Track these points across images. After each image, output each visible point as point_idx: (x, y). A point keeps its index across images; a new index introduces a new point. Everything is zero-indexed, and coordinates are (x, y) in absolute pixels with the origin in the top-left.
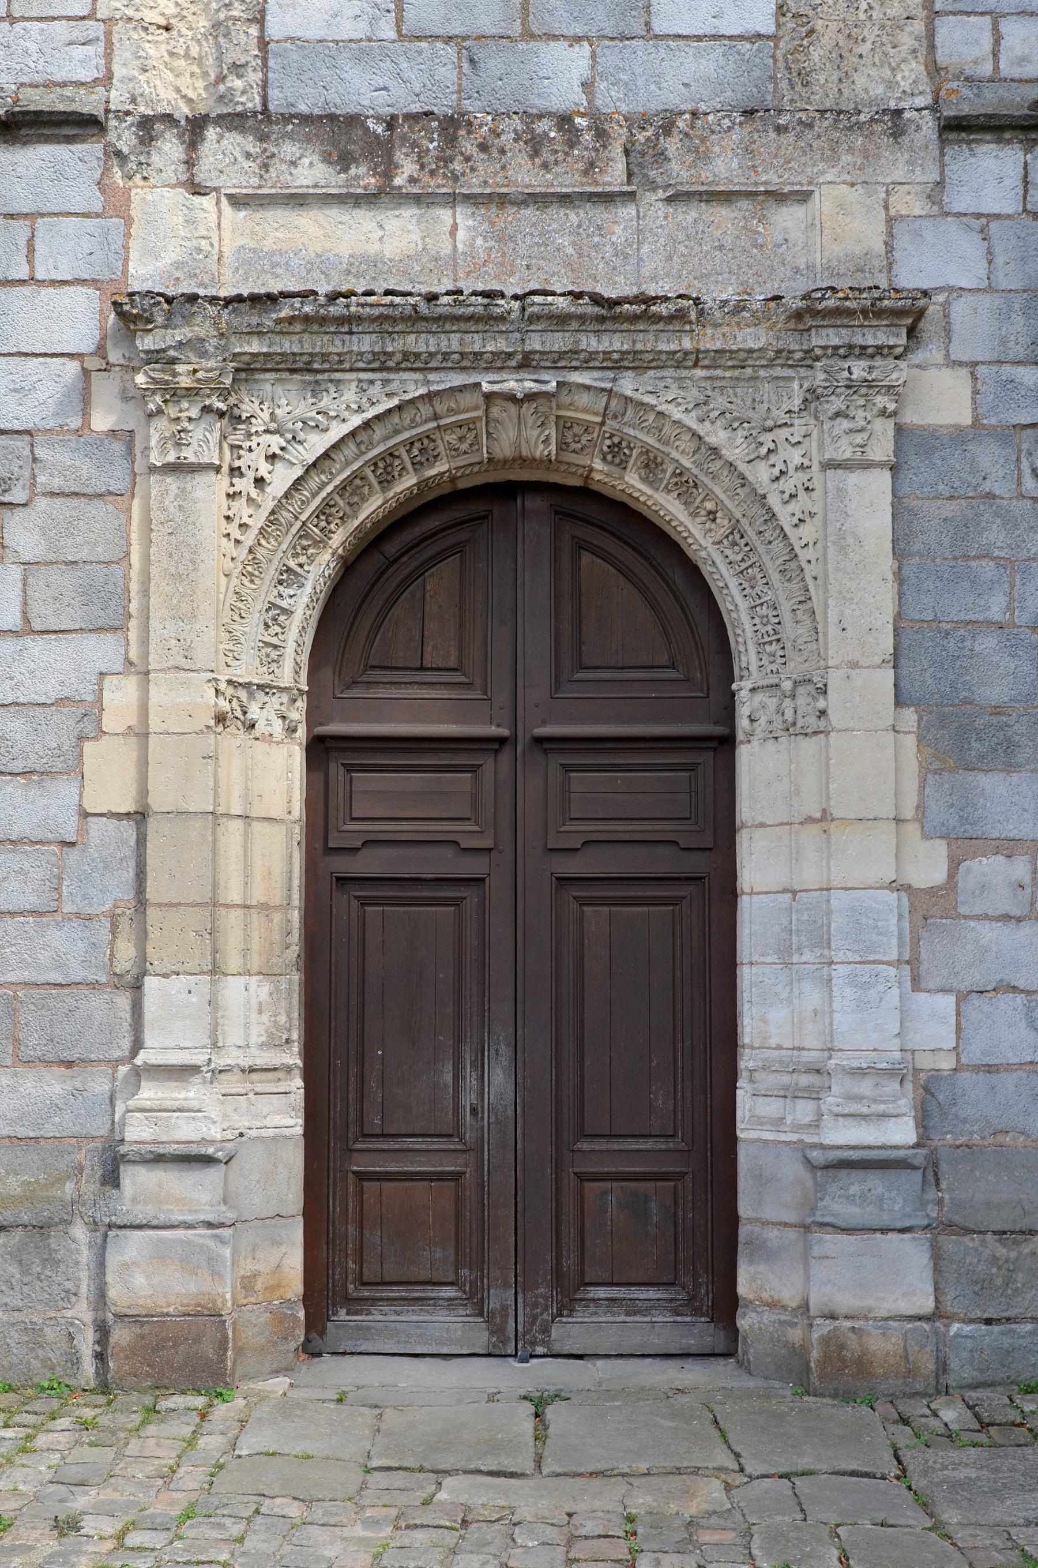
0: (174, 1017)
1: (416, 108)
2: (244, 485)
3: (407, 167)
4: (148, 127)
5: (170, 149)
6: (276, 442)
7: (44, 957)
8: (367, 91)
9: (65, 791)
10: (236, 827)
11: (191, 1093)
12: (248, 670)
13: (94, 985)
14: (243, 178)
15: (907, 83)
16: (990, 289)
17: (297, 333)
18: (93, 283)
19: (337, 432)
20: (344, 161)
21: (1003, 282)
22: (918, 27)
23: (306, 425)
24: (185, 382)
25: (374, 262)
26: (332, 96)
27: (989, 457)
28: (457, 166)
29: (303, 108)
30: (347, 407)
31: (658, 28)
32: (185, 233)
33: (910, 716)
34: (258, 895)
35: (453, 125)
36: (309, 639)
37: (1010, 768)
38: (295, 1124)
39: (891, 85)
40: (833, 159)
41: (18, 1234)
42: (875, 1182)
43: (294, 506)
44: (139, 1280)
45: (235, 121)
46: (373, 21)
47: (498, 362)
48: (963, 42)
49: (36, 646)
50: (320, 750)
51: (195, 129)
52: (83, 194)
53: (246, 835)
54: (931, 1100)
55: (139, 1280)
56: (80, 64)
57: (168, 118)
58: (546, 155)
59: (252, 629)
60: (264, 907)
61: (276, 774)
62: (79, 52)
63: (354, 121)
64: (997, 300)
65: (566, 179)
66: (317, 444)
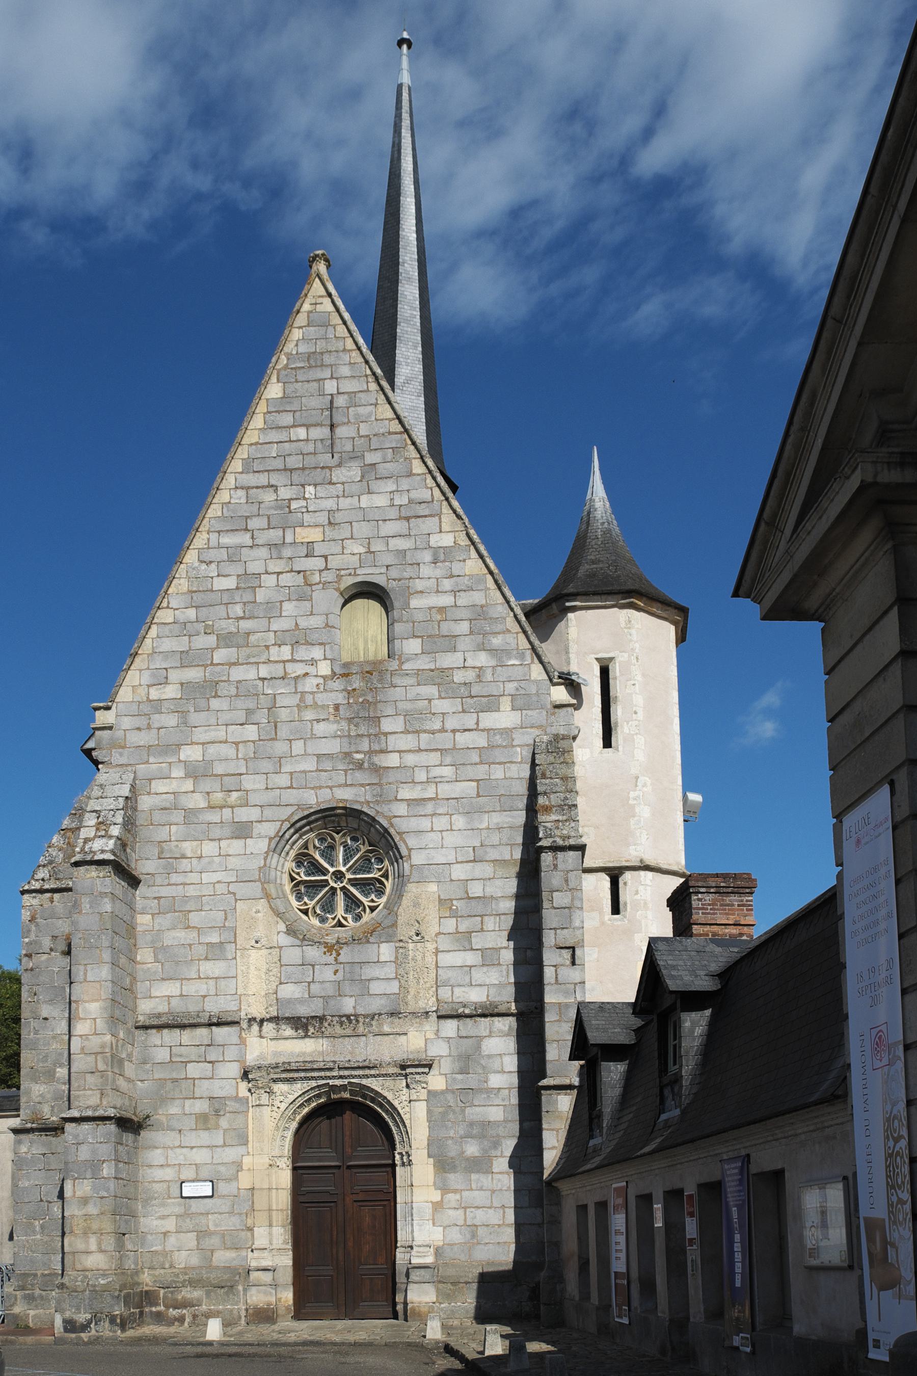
0: (261, 1236)
1: (313, 1014)
2: (275, 1109)
3: (311, 1030)
4: (251, 1020)
5: (255, 1027)
6: (282, 1098)
7: (230, 1223)
8: (303, 1011)
9: (234, 1184)
10: (274, 1191)
11: (266, 1254)
12: (277, 1152)
13: (242, 1230)
14: (273, 1034)
15: (431, 1005)
16: (450, 1056)
17: (288, 1072)
18: (238, 1061)
19: (297, 1095)
20: (297, 1029)
21: (453, 1054)
22: (434, 989)
23: (289, 1094)
24: (260, 1085)
25: (304, 1054)
26: (293, 1012)
27: (450, 1097)
28: (323, 1029)
29: (287, 1015)
30: (299, 1088)
31: (371, 992)
32: (261, 1048)
33: (432, 1160)
34: (280, 1207)
35: (322, 1019)
36: (291, 1143)
37: (455, 1172)
38: (290, 1263)
39: (427, 1004)
40: (412, 1026)
41: (226, 1289)
42: (422, 1271)
43: (287, 1112)
44: (254, 1298)
45: (270, 1020)
46: (303, 993)
47: (334, 1077)
48: (445, 993)
49: (227, 1149)
50: (295, 1169)
51: (262, 1021)
52: (235, 1040)
53: (556, 934)
54: (438, 1252)
55: (254, 1298)
56: (233, 1007)
57: (254, 1019)
58: (344, 1026)
59: (278, 1142)
60: (281, 1210)
61: (285, 1177)
62: (233, 1003)
63: (299, 1018)
64: (451, 1058)
65: (349, 1031)
66: (292, 1098)
